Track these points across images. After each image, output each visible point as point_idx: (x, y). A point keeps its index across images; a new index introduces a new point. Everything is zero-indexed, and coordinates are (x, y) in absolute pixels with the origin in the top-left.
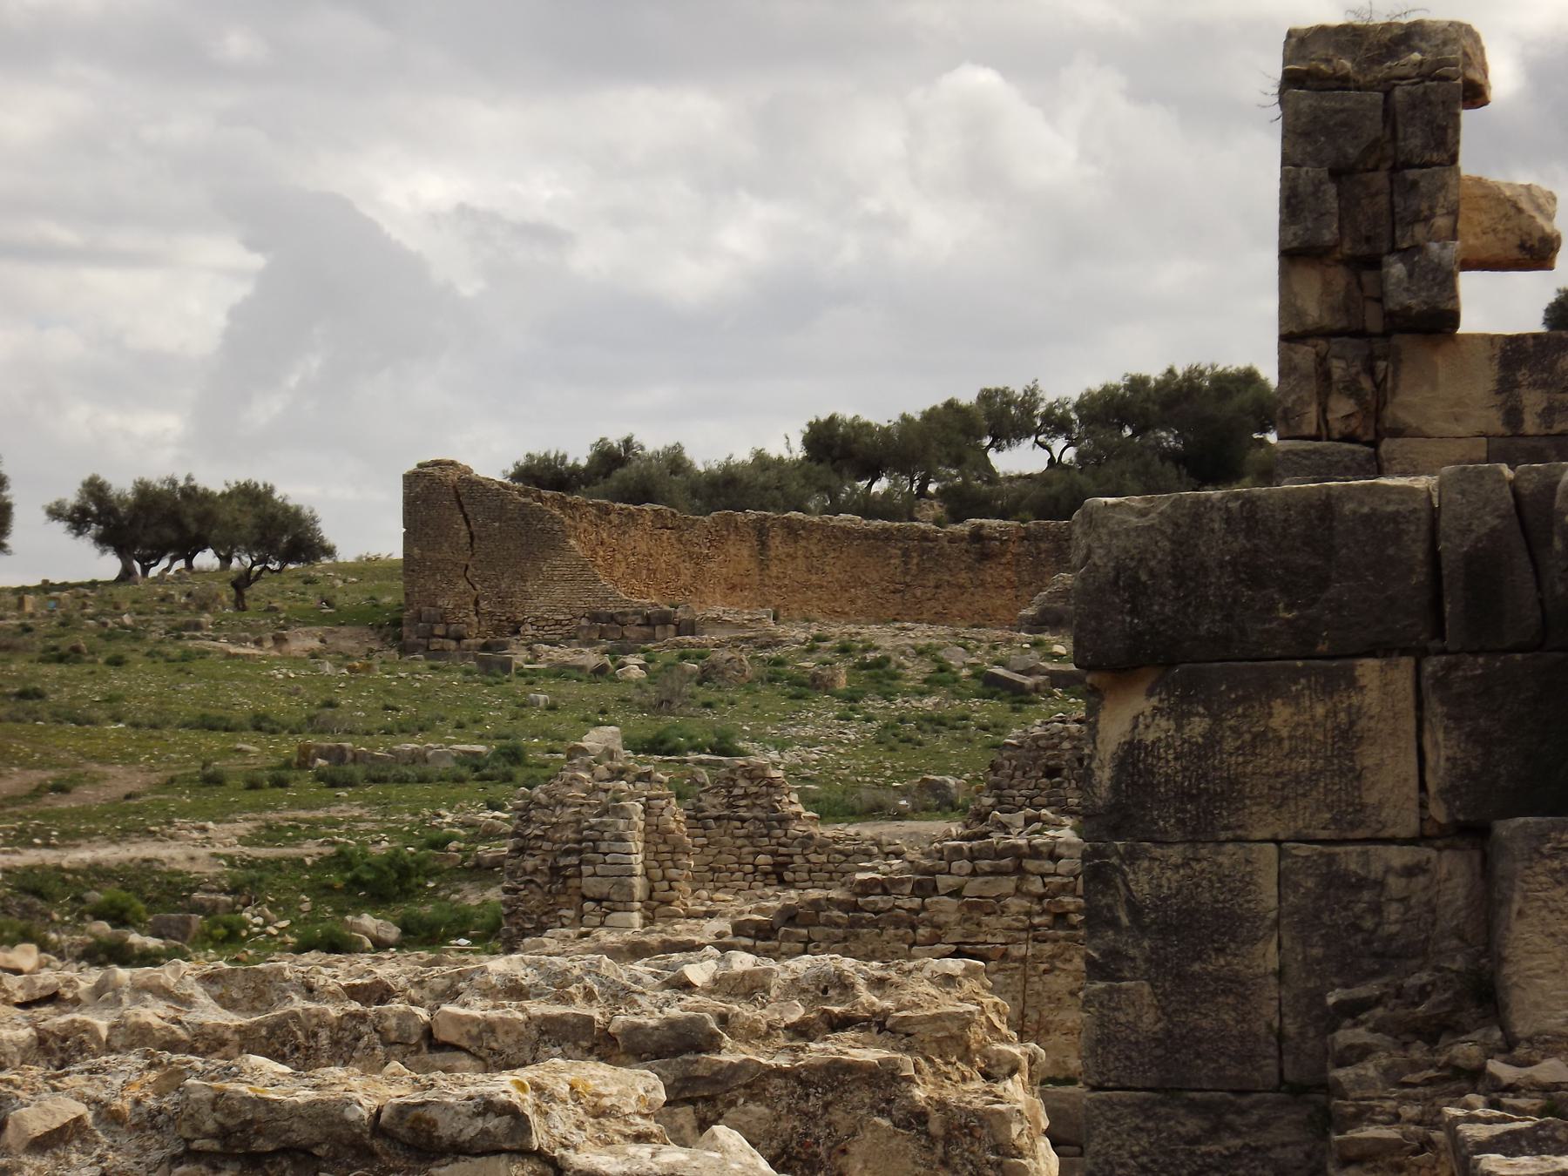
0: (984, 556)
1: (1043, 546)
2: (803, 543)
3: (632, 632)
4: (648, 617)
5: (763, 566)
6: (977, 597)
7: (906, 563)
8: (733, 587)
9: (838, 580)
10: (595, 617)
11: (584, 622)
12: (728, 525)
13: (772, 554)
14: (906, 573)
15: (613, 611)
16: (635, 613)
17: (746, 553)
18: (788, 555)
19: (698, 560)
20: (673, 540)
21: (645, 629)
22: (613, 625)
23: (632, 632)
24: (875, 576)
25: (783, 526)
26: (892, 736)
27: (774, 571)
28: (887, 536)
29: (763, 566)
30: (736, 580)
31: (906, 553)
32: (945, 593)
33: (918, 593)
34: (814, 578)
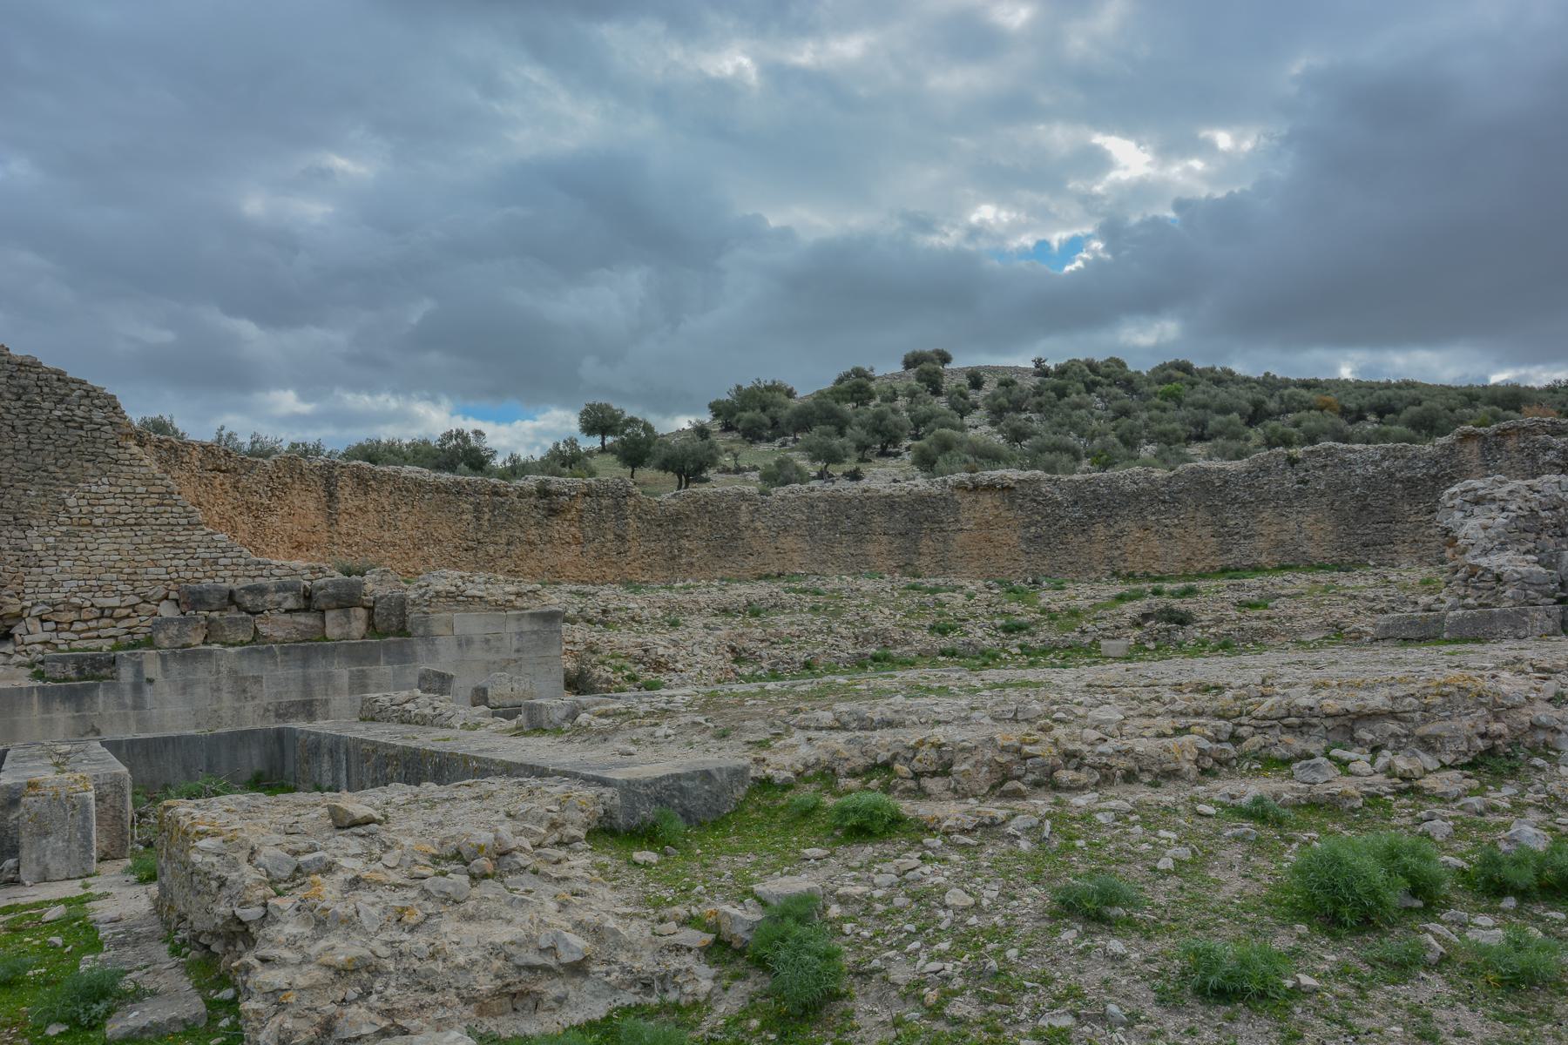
0: (553, 512)
1: (604, 502)
2: (374, 495)
3: (276, 627)
4: (308, 596)
5: (332, 521)
6: (546, 554)
7: (478, 519)
8: (299, 546)
9: (411, 537)
10: (192, 600)
11: (167, 610)
12: (292, 470)
13: (341, 506)
14: (478, 528)
15: (229, 584)
16: (282, 588)
17: (311, 505)
18: (359, 508)
19: (257, 513)
20: (227, 486)
21: (302, 619)
22: (233, 613)
23: (276, 627)
24: (448, 533)
25: (352, 475)
26: (1507, 827)
27: (344, 526)
28: (459, 490)
29: (332, 521)
30: (302, 537)
31: (477, 509)
32: (517, 550)
33: (491, 549)
34: (387, 535)
